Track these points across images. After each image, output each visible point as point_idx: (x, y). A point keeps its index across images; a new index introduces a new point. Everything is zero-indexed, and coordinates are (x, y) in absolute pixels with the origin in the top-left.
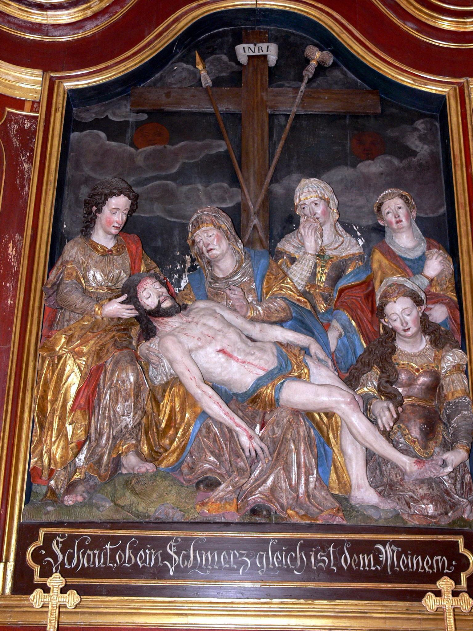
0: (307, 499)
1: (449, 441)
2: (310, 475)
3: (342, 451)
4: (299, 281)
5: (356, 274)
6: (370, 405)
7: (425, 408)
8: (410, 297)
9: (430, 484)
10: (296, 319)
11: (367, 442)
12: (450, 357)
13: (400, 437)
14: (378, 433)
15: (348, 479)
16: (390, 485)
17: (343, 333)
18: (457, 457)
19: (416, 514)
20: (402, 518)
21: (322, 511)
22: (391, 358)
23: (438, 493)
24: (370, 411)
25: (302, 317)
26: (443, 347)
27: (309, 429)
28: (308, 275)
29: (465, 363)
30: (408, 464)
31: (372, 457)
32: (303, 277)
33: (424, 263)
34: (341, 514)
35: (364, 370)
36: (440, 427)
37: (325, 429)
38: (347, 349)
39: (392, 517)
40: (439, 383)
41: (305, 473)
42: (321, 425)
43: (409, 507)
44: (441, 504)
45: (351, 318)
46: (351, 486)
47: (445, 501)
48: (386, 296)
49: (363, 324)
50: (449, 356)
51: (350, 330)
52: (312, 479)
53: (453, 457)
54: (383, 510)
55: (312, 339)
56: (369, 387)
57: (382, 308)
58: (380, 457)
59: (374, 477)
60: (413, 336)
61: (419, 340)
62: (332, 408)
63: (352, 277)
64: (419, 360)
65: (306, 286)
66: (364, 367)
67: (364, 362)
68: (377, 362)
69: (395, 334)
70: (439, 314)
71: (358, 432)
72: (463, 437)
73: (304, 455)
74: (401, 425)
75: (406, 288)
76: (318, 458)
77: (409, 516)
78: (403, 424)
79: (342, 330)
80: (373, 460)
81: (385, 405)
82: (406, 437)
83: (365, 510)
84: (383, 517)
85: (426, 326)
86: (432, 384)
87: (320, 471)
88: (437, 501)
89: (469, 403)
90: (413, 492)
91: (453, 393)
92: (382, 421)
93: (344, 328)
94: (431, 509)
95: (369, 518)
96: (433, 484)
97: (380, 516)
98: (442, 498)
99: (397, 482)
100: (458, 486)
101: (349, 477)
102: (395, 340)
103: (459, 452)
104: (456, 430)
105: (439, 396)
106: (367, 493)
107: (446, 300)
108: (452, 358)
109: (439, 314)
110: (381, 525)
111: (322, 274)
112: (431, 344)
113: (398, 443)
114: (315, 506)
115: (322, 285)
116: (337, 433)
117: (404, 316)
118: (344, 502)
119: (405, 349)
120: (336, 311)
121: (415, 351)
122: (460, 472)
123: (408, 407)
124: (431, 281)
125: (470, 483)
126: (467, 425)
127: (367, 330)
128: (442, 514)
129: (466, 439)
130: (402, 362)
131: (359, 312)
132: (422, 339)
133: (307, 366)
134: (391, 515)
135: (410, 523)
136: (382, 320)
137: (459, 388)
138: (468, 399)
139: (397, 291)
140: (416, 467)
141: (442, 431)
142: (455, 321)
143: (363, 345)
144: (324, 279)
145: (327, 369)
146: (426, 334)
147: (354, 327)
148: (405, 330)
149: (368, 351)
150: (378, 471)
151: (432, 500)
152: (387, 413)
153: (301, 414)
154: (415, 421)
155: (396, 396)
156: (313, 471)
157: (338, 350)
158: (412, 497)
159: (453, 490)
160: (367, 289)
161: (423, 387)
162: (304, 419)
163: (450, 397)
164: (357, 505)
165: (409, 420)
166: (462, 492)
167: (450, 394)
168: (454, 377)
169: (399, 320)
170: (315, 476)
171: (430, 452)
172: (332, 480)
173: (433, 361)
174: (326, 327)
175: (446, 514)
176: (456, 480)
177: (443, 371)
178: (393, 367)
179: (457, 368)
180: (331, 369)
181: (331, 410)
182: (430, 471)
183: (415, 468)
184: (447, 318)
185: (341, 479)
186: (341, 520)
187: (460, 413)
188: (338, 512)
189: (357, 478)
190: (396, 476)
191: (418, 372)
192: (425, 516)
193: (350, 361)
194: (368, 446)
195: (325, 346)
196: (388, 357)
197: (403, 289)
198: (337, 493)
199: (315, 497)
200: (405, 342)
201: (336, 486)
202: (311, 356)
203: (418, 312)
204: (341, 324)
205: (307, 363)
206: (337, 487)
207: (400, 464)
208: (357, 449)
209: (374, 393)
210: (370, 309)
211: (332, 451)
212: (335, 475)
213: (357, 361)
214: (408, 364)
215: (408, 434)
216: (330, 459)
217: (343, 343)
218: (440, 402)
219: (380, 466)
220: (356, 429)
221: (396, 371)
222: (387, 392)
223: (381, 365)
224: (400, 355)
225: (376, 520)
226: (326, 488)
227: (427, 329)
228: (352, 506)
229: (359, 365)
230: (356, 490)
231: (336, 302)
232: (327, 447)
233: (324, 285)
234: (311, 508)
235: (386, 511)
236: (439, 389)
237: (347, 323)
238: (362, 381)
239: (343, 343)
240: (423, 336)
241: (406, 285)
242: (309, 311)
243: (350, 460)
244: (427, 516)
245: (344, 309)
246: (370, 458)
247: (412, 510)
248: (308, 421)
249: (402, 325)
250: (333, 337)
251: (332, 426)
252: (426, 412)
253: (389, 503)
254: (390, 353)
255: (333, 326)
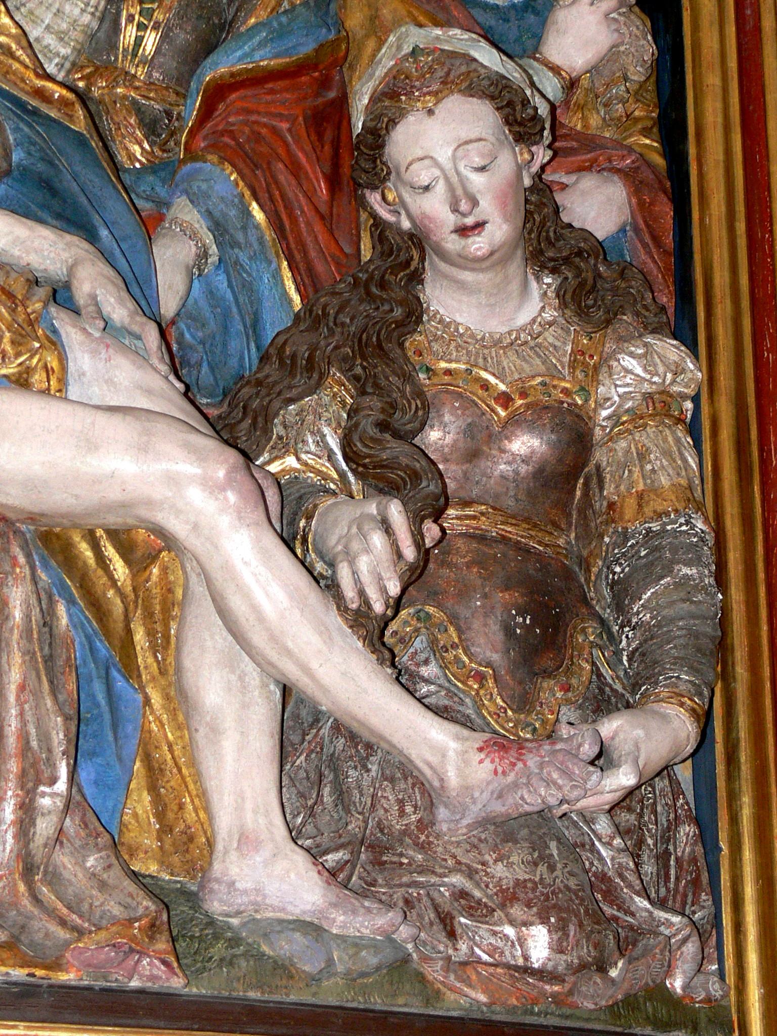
0: (22, 887)
1: (618, 687)
2: (38, 782)
3: (180, 701)
4: (50, 40)
5: (281, 33)
6: (309, 518)
7: (526, 551)
8: (492, 98)
9: (538, 846)
10: (25, 174)
11: (288, 653)
12: (634, 362)
13: (423, 656)
14: (335, 620)
15: (202, 815)
16: (377, 849)
17: (214, 249)
18: (652, 735)
19: (479, 961)
20: (421, 978)
21: (80, 932)
22: (401, 345)
23: (572, 883)
24: (305, 541)
25: (51, 163)
26: (608, 322)
27: (50, 597)
28: (86, 18)
29: (690, 391)
30: (451, 754)
31: (304, 734)
32: (64, 26)
33: (543, 23)
34: (162, 945)
35: (290, 387)
36: (583, 630)
37: (118, 607)
38: (226, 316)
39: (378, 969)
40: (585, 464)
41: (23, 775)
42: (99, 590)
43: (452, 935)
44: (581, 925)
45: (247, 193)
46: (210, 844)
47: (598, 917)
48: (394, 98)
49: (293, 220)
50: (632, 355)
51: (240, 237)
52: (49, 799)
53: (640, 733)
54: (342, 938)
55: (85, 245)
56: (313, 444)
57: (376, 137)
58: (338, 727)
59: (312, 814)
60: (493, 260)
61: (515, 286)
62: (149, 503)
63: (261, 45)
64: (509, 361)
65: (75, 67)
66: (292, 374)
67: (294, 357)
68: (345, 359)
69: (422, 259)
70: (597, 206)
71: (255, 608)
72: (678, 662)
73: (20, 704)
74: (431, 610)
75: (474, 66)
76: (78, 722)
77: (447, 969)
78: (439, 606)
79: (209, 239)
80: (303, 728)
81: (372, 508)
82: (450, 656)
83: (265, 935)
84: (340, 968)
85: (545, 239)
86: (560, 461)
87: (85, 775)
88: (568, 910)
89: (702, 540)
90: (471, 873)
91: (640, 496)
92: (354, 573)
93: (218, 227)
94: (539, 945)
95: (283, 969)
96: (553, 845)
97: (330, 962)
98: (586, 909)
99: (405, 832)
100: (649, 868)
101: (207, 809)
102: (421, 282)
103: (665, 718)
104: (649, 634)
105: (582, 511)
106: (280, 867)
107: (623, 158)
108: (640, 367)
109: (597, 206)
110: (333, 1001)
111: (141, 27)
112: (563, 305)
113: (415, 677)
114: (51, 913)
115: (141, 73)
116: (167, 628)
117: (462, 168)
118: (178, 913)
119: (459, 319)
120: (189, 166)
121: (496, 326)
122: (654, 812)
123: (460, 543)
124: (571, 85)
125: (694, 860)
126: (693, 616)
127: (311, 246)
128: (583, 966)
129: (693, 670)
130: (443, 365)
131: (284, 177)
132: (525, 285)
133: (54, 342)
134: (374, 961)
135: (451, 996)
136: (373, 198)
137: (664, 481)
138: (700, 525)
139: (440, 73)
140: (488, 765)
141: (592, 645)
142: (655, 239)
143: (290, 301)
144: (151, 41)
145: (140, 361)
146: (543, 267)
147: (257, 227)
148: (463, 231)
149: (311, 318)
150: (326, 791)
151: (547, 909)
152: (378, 539)
153: (17, 532)
154: (485, 596)
155: (415, 477)
156: (54, 767)
157: (191, 317)
158: (463, 894)
159: (632, 877)
160: (317, 95)
161: (524, 469)
162: (28, 556)
163: (629, 513)
164: (235, 921)
165: (464, 593)
166: (663, 891)
167: (631, 502)
168: (648, 436)
169: (440, 188)
170: (61, 786)
171: (544, 722)
172: (135, 815)
173: (566, 372)
174: (150, 225)
175: (602, 968)
176: (640, 842)
177: (605, 413)
178: (408, 378)
179: (659, 405)
180: (155, 361)
181: (143, 512)
182: (543, 784)
183: (481, 770)
184: (622, 230)
185: (171, 815)
186: (160, 970)
187: (668, 570)
188: (151, 938)
189: (239, 809)
190: (402, 813)
191: (505, 407)
192: (516, 968)
193: (233, 362)
194: (293, 673)
195: (139, 287)
196: (389, 339)
197: (464, 69)
198: (153, 868)
199: (54, 878)
200: (462, 286)
201: (150, 842)
202: (77, 312)
203: (519, 169)
204: (209, 214)
205: (55, 331)
206: (156, 844)
207: (420, 755)
208: (244, 689)
209: (326, 477)
210: (327, 168)
211: (140, 697)
212: (147, 798)
213: (264, 359)
214: (469, 372)
215: (454, 646)
216: (130, 728)
217: (211, 293)
218: (587, 534)
219: (335, 770)
220: (247, 596)
221: (419, 393)
222: (384, 462)
223: (358, 370)
224: (436, 339)
225: (314, 980)
226: (104, 840)
227: (551, 244)
228: (211, 922)
229: (272, 370)
230: (233, 856)
231: (192, 133)
232: (120, 683)
233: (149, 75)
234: (36, 925)
235: (356, 944)
236: (586, 484)
237: (233, 213)
238: (278, 430)
239: (211, 293)
240: (531, 278)
241: (476, 55)
242: (80, 140)
243: (215, 730)
244: (527, 970)
245: (223, 159)
246: (295, 738)
247: (463, 947)
248: (46, 566)
249: (455, 210)
250: (172, 264)
251: (148, 600)
252: (531, 568)
253: (369, 910)
254: (400, 324)
255: (174, 220)
